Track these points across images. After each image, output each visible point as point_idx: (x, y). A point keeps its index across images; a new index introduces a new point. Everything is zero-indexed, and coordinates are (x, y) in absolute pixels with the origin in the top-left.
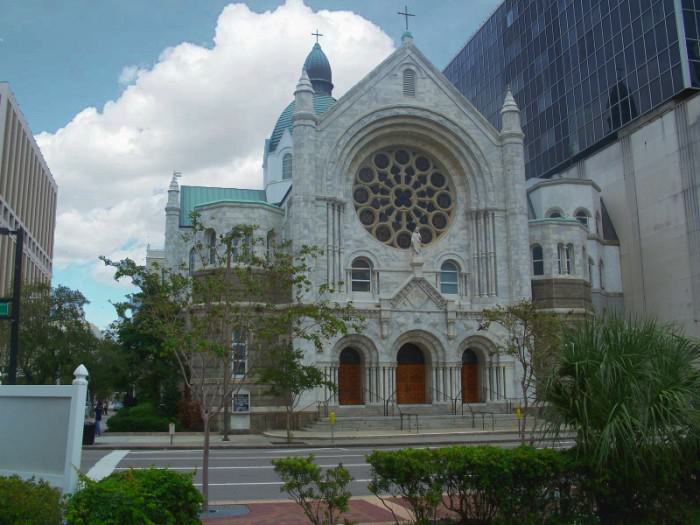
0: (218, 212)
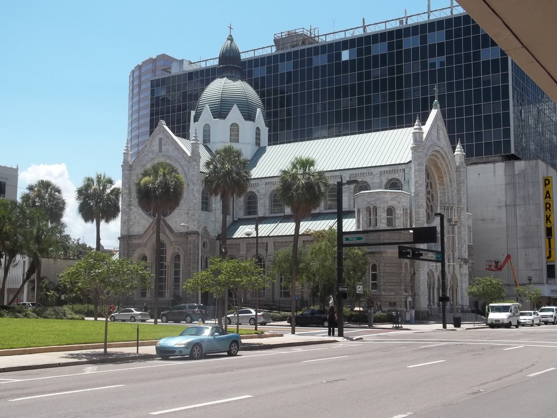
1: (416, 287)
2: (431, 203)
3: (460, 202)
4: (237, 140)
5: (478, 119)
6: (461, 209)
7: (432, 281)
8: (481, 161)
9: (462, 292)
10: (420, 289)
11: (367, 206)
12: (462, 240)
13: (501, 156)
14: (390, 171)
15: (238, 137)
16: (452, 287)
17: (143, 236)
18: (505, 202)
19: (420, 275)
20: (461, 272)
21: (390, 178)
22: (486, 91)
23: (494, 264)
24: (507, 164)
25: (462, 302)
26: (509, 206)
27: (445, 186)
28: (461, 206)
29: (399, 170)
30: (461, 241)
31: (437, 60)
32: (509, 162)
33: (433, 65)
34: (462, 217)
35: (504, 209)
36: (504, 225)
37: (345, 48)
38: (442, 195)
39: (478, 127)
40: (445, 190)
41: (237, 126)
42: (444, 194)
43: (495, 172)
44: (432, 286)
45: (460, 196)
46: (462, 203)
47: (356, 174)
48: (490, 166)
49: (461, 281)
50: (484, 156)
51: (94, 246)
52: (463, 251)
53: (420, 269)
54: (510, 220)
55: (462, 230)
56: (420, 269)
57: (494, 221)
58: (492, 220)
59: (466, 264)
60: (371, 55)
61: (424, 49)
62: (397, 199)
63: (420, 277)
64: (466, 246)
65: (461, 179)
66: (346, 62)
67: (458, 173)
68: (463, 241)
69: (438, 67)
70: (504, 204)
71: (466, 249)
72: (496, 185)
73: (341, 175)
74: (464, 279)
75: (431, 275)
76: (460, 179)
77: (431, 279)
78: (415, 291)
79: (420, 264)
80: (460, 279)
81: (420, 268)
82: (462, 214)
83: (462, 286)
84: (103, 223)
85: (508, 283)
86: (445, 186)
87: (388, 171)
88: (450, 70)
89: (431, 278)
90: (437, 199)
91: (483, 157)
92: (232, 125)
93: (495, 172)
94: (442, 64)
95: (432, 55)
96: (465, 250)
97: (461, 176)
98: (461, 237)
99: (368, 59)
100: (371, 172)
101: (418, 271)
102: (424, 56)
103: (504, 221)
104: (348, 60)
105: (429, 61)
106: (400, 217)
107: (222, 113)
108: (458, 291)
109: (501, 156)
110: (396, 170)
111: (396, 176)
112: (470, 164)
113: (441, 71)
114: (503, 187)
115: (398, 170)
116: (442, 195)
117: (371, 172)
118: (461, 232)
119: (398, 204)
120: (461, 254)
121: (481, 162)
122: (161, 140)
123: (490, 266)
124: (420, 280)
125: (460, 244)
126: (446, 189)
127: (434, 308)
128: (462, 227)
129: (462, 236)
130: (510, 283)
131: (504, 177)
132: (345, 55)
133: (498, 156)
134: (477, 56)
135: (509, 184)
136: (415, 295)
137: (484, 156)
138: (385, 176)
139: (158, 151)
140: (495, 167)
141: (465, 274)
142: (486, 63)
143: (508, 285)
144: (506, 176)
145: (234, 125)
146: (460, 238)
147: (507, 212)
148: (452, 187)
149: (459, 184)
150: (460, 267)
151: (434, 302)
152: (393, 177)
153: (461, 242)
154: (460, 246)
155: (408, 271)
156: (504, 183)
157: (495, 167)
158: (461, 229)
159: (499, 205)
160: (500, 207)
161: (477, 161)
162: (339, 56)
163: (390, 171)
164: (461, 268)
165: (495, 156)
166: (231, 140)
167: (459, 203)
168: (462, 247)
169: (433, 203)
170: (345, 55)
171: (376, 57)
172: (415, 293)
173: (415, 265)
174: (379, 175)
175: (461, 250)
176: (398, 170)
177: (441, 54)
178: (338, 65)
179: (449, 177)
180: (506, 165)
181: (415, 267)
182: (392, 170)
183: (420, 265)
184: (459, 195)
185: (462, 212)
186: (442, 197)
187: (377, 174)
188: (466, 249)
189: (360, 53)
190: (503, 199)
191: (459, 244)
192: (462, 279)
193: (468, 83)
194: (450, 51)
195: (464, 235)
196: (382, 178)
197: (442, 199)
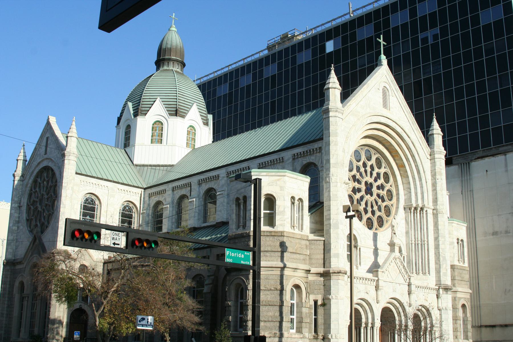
0: (279, 180)
4: (160, 140)
5: (482, 100)
8: (488, 153)
11: (236, 197)
14: (304, 152)
15: (162, 137)
17: (23, 262)
21: (305, 162)
22: (490, 62)
29: (315, 150)
31: (429, 34)
33: (425, 40)
37: (329, 39)
39: (483, 108)
41: (160, 124)
43: (506, 166)
47: (265, 162)
50: (492, 147)
51: (211, 285)
60: (357, 41)
61: (414, 23)
62: (278, 182)
66: (331, 53)
69: (430, 41)
71: (447, 270)
72: (509, 184)
73: (249, 167)
87: (302, 153)
88: (445, 43)
91: (491, 149)
92: (155, 123)
93: (506, 166)
94: (435, 37)
95: (424, 29)
99: (353, 46)
100: (282, 158)
102: (414, 32)
104: (333, 51)
105: (420, 36)
106: (284, 211)
107: (144, 109)
110: (312, 150)
111: (313, 160)
112: (475, 159)
113: (435, 46)
115: (313, 150)
117: (282, 158)
119: (281, 190)
121: (489, 155)
122: (47, 138)
132: (330, 47)
134: (476, 20)
138: (298, 161)
139: (44, 153)
140: (506, 160)
142: (487, 27)
145: (157, 123)
150: (437, 298)
152: (308, 161)
157: (506, 160)
161: (484, 154)
162: (323, 48)
163: (304, 152)
165: (507, 145)
166: (153, 141)
170: (330, 47)
171: (362, 42)
174: (291, 160)
176: (313, 150)
177: (433, 25)
178: (322, 58)
182: (307, 151)
187: (288, 159)
189: (344, 41)
193: (467, 56)
194: (443, 21)
196: (295, 164)
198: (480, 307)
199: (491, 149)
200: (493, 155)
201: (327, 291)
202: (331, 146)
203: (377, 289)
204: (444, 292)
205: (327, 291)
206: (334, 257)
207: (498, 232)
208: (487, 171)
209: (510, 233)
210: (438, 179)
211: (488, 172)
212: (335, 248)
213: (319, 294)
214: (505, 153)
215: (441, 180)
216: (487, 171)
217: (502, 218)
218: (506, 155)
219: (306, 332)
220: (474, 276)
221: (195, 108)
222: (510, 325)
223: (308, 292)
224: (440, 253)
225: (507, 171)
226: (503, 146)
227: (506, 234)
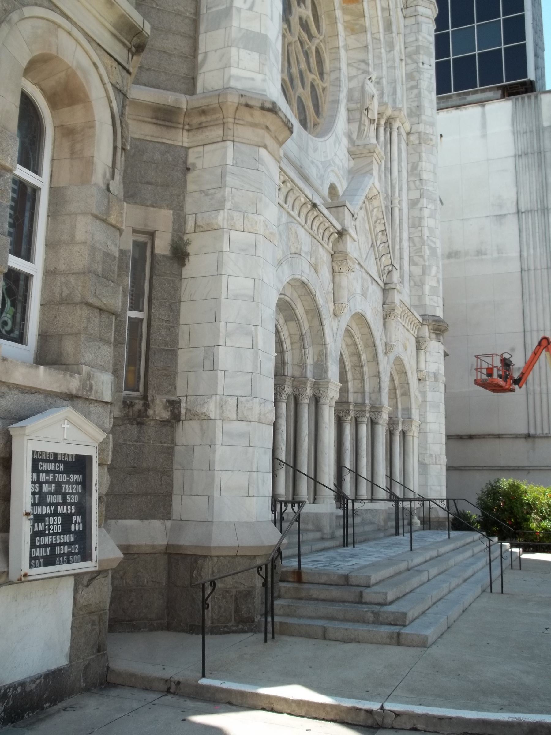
1: (183, 357)
2: (317, 41)
3: (418, 116)
6: (420, 138)
7: (310, 360)
9: (423, 444)
10: (214, 369)
12: (426, 247)
13: (498, 88)
16: (392, 423)
18: (515, 203)
19: (220, 263)
20: (422, 366)
23: (497, 363)
24: (526, 99)
25: (425, 485)
26: (525, 212)
27: (369, 36)
28: (421, 128)
30: (420, 250)
32: (530, 96)
34: (424, 165)
35: (511, 225)
36: (515, 267)
38: (354, 72)
40: (367, 51)
42: (363, 66)
43: (484, 125)
44: (309, 392)
45: (419, 96)
46: (423, 117)
48: (474, 111)
49: (420, 399)
52: (427, 289)
53: (221, 218)
54: (532, 251)
55: (426, 213)
56: (221, 218)
57: (484, 257)
58: (479, 253)
59: (438, 339)
63: (218, 275)
64: (438, 272)
65: (420, 38)
67: (412, 20)
68: (427, 252)
70: (514, 210)
72: (488, 160)
74: (430, 396)
75: (305, 327)
76: (417, 40)
77: (303, 347)
78: (180, 382)
79: (223, 176)
80: (419, 395)
81: (220, 207)
82: (423, 154)
83: (423, 421)
84: (335, 494)
85: (525, 432)
86: (369, 36)
89: (308, 340)
90: (338, 79)
96: (434, 284)
97: (419, 31)
98: (422, 237)
101: (211, 228)
103: (515, 254)
108: (409, 439)
109: (498, 88)
114: (510, 164)
116: (354, 72)
118: (421, 218)
120: (420, 297)
123: (490, 373)
124: (217, 300)
125: (416, 264)
126: (370, 47)
127: (317, 517)
128: (424, 201)
129: (426, 232)
130: (532, 432)
131: (509, 139)
133: (491, 89)
135: (526, 154)
136: (176, 418)
137: (452, 93)
140: (484, 114)
141: (436, 376)
143: (528, 436)
144: (515, 133)
146: (417, 240)
147: (520, 230)
148: (391, 46)
149: (415, 57)
150: (418, 348)
151: (316, 481)
153: (422, 257)
154: (417, 270)
155: (90, 162)
156: (512, 153)
157: (484, 114)
158: (421, 209)
159: (500, 213)
160: (500, 216)
164: (422, 352)
167: (415, 120)
168: (424, 273)
169: (321, 38)
172: (174, 405)
173: (190, 187)
175: (421, 285)
179: (383, 9)
180: (515, 107)
181: (189, 208)
183: (222, 186)
184: (415, 91)
185: (423, 149)
186: (354, 77)
188: (438, 282)
190: (510, 195)
191: (412, 262)
192: (424, 393)
195: (431, 230)
197: (354, 84)
198: (548, 393)
199: (450, 97)
200: (457, 107)
201: (201, 192)
202: (69, 645)
203: (336, 268)
204: (431, 334)
205: (201, 192)
206: (245, 48)
207: (460, 252)
208: (441, 136)
209: (486, 254)
210: (423, 63)
211: (443, 138)
212: (251, 8)
213: (160, 207)
214: (482, 103)
215: (429, 67)
216: (441, 136)
217: (471, 225)
218: (484, 106)
219: (103, 369)
220: (533, 303)
221: (208, 626)
222: (479, 435)
223: (123, 149)
224: (425, 238)
225: (484, 136)
226: (476, 92)
227: (478, 255)
